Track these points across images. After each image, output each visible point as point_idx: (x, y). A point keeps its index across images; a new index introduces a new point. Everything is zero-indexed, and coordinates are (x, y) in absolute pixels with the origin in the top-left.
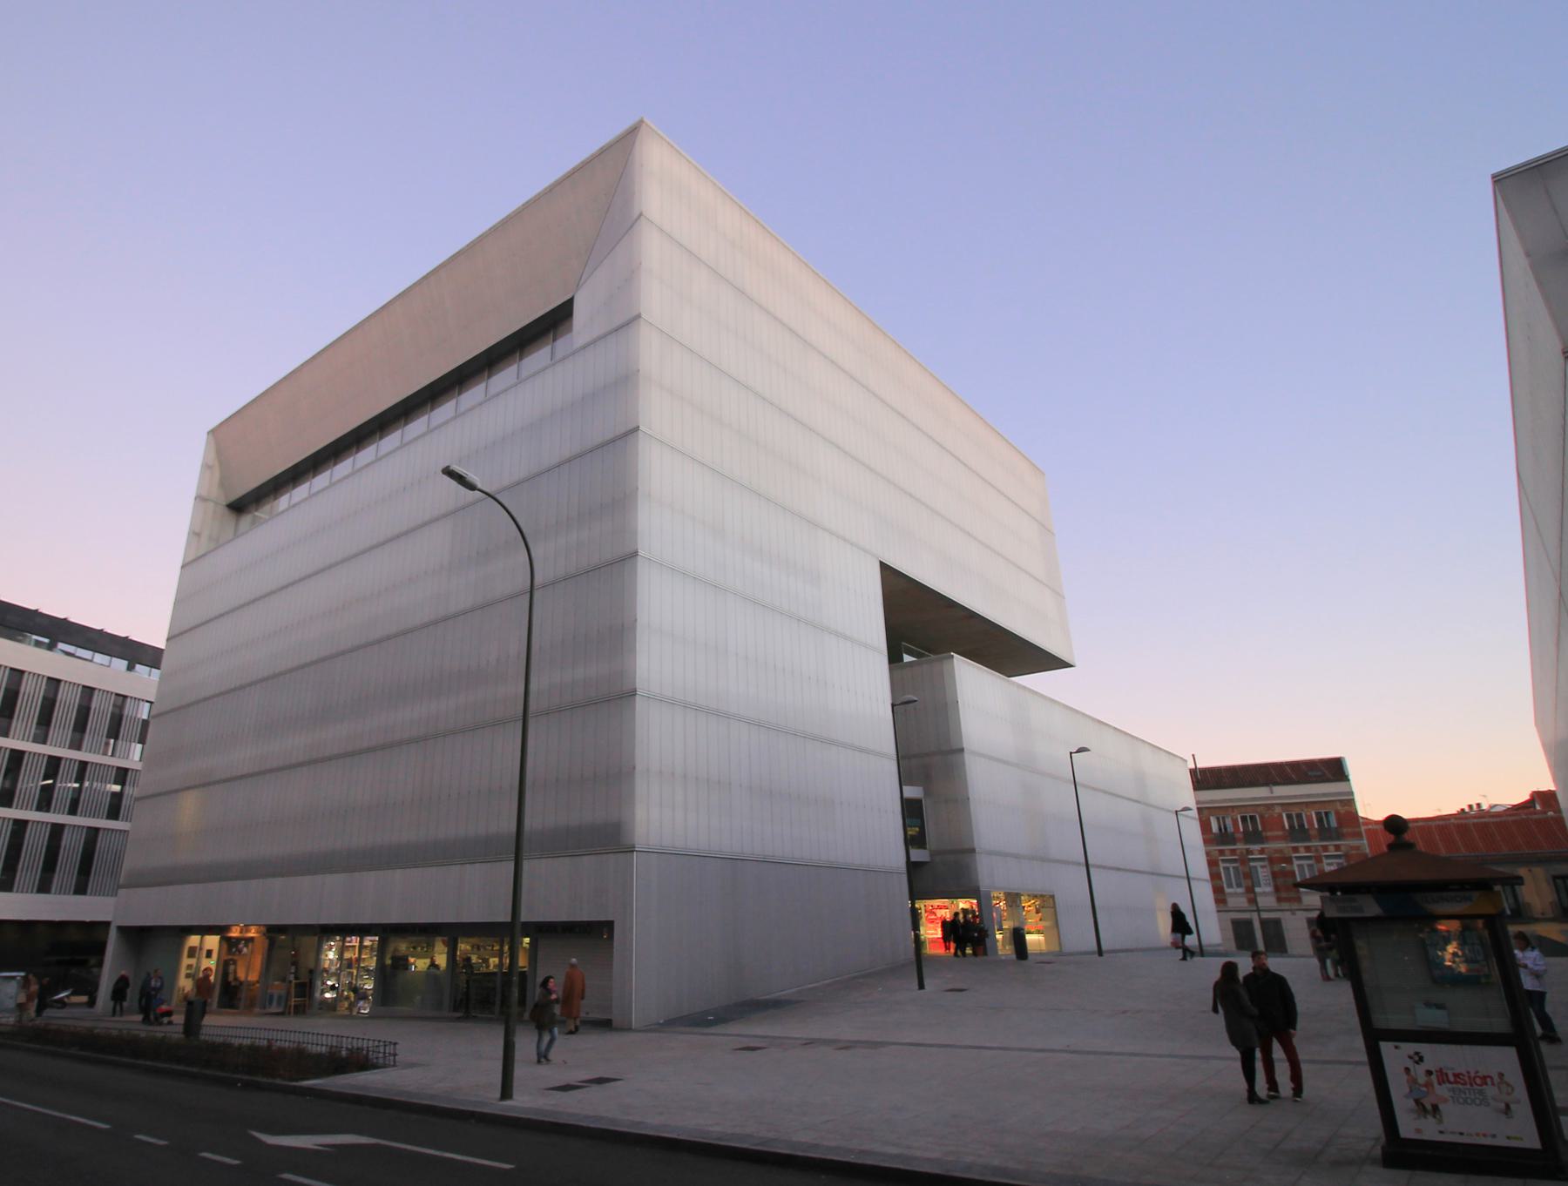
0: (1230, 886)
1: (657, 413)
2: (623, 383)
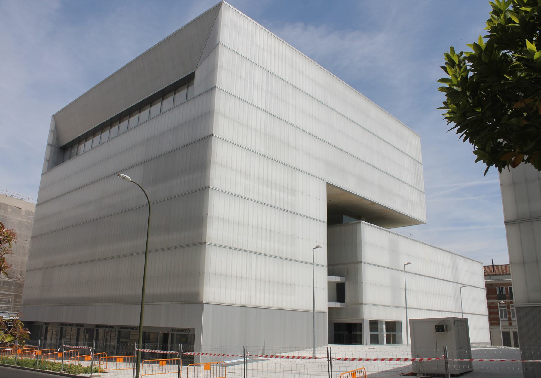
0: (502, 317)
1: (222, 127)
2: (207, 115)
